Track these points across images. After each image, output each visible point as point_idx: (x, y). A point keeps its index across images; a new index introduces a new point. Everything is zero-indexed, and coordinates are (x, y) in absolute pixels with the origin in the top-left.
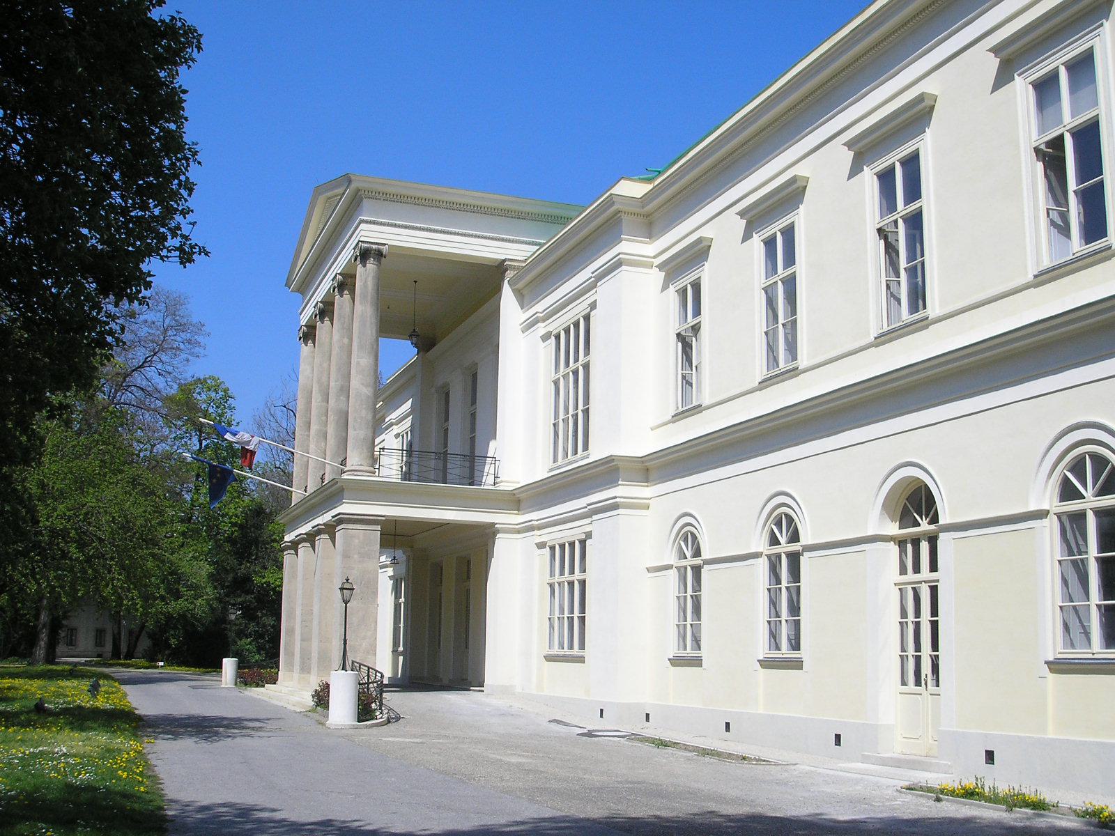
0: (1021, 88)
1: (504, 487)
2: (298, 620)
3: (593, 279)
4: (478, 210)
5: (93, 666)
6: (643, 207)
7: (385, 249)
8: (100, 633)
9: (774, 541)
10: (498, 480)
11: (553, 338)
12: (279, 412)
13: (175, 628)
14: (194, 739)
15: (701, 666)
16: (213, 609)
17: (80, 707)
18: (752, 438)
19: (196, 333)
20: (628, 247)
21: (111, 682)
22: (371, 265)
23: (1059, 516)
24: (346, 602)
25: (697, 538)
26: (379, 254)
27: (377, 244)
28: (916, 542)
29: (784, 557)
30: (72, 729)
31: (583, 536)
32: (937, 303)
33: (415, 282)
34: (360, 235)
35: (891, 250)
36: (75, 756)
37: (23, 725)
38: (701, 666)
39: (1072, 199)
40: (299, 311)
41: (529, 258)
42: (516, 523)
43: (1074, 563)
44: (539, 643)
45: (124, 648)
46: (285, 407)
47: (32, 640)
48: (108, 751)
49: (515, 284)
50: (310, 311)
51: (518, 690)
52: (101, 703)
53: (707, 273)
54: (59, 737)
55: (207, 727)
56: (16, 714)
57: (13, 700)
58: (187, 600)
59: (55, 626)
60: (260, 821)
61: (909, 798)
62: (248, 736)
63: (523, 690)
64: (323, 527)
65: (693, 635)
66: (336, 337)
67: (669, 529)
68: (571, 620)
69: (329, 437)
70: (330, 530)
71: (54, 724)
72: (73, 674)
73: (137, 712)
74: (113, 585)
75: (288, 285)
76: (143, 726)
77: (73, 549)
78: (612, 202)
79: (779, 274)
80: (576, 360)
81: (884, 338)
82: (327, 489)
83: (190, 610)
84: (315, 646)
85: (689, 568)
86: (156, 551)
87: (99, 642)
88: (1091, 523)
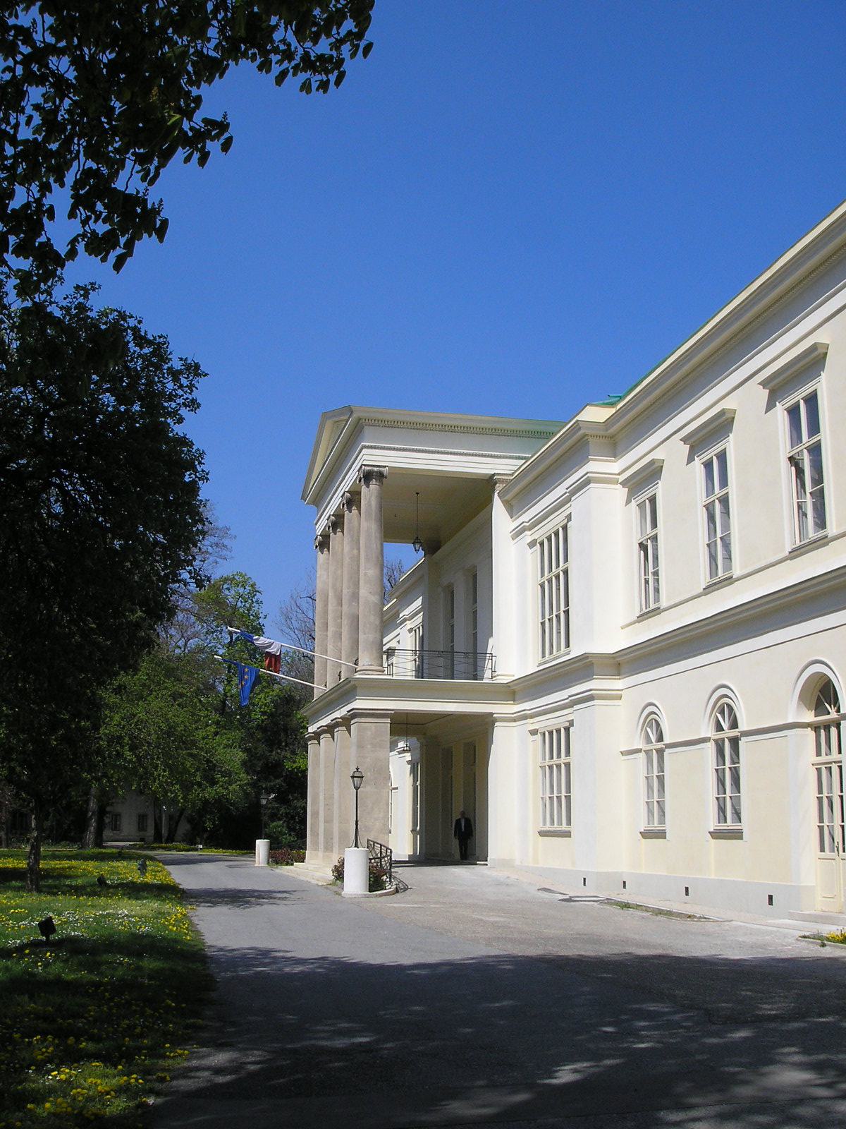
3: (567, 494)
4: (467, 430)
6: (607, 430)
7: (385, 470)
8: (142, 819)
9: (719, 728)
10: (495, 674)
11: (538, 545)
12: (304, 604)
13: (211, 813)
14: (229, 906)
15: (570, 837)
16: (246, 794)
17: (132, 882)
18: (708, 635)
20: (596, 466)
22: (374, 485)
24: (357, 788)
25: (733, 709)
26: (381, 476)
27: (378, 466)
28: (827, 727)
30: (129, 898)
31: (567, 724)
32: (834, 523)
33: (417, 494)
35: (800, 473)
36: (134, 916)
38: (570, 837)
41: (516, 471)
42: (513, 712)
44: (535, 820)
45: (164, 831)
46: (310, 598)
47: (82, 826)
48: (160, 913)
49: (504, 496)
51: (517, 863)
52: (149, 879)
53: (661, 489)
55: (240, 897)
57: (77, 877)
58: (222, 786)
59: (102, 812)
60: (275, 958)
61: (803, 944)
62: (274, 904)
63: (521, 862)
64: (340, 720)
65: (733, 806)
66: (347, 549)
67: (637, 719)
68: (559, 798)
70: (346, 722)
72: (120, 856)
73: (180, 887)
75: (304, 498)
76: (187, 897)
77: (128, 754)
78: (577, 428)
79: (804, 443)
80: (558, 566)
81: (796, 553)
82: (343, 686)
83: (226, 795)
85: (726, 740)
86: (194, 751)
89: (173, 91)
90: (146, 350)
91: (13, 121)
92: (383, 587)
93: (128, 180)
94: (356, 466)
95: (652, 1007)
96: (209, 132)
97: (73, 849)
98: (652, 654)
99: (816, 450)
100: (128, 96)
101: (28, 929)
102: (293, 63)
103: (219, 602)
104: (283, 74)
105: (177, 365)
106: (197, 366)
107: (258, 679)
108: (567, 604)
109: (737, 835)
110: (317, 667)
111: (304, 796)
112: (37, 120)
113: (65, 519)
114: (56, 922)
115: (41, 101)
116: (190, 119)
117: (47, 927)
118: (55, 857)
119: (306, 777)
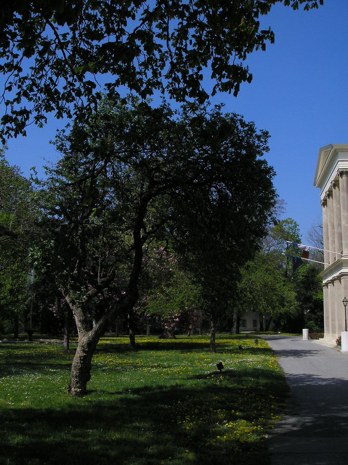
2: (330, 313)
5: (254, 334)
8: (255, 322)
12: (318, 229)
19: (282, 204)
21: (262, 340)
22: (344, 177)
24: (345, 306)
34: (339, 166)
36: (254, 362)
37: (236, 353)
40: (320, 195)
45: (264, 327)
47: (231, 325)
52: (259, 346)
54: (249, 356)
55: (298, 353)
56: (233, 350)
57: (230, 346)
58: (287, 307)
59: (239, 319)
69: (336, 243)
70: (339, 278)
71: (246, 352)
72: (247, 337)
73: (272, 349)
74: (262, 305)
76: (275, 354)
77: (248, 294)
82: (336, 263)
86: (276, 293)
87: (255, 325)
90: (245, 129)
91: (184, 44)
93: (234, 60)
94: (336, 170)
97: (227, 335)
101: (210, 367)
103: (282, 231)
105: (258, 133)
112: (194, 41)
114: (223, 364)
117: (220, 366)
118: (220, 338)
119: (322, 302)
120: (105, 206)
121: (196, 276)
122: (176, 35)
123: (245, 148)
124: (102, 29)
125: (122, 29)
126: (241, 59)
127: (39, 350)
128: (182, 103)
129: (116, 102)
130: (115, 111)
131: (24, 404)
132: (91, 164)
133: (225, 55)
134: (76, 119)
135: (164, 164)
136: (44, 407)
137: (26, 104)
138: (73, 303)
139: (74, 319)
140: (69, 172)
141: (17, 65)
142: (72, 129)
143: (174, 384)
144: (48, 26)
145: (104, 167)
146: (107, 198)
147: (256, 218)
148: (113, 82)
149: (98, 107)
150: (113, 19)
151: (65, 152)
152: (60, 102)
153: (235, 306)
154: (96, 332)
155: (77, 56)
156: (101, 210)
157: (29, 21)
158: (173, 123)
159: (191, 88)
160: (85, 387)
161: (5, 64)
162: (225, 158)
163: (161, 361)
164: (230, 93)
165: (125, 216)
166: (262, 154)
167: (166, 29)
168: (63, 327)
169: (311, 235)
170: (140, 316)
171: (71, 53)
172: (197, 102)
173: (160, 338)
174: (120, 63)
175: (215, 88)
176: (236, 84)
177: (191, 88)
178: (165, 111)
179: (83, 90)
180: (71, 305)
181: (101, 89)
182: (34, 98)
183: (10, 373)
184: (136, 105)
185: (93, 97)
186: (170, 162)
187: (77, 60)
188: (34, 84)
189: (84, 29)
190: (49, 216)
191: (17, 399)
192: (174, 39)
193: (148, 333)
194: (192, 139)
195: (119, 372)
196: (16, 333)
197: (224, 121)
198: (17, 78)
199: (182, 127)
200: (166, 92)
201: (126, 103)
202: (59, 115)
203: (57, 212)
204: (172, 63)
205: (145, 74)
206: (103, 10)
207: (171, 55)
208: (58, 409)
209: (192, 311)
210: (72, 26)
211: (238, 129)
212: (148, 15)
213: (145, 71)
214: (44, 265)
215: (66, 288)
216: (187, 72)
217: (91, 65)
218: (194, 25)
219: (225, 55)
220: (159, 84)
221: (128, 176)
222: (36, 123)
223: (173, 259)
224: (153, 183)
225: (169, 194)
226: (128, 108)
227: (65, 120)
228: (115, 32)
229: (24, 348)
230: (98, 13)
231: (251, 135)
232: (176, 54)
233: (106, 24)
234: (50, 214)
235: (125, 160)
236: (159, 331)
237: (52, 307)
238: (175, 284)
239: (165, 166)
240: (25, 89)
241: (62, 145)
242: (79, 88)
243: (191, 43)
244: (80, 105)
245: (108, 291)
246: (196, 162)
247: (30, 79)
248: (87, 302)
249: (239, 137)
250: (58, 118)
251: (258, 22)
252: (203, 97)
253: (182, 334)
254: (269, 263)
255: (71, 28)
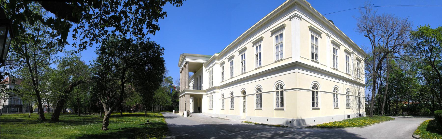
0: (274, 37)
1: (203, 90)
4: (199, 57)
8: (159, 108)
9: (231, 96)
12: (179, 80)
15: (262, 110)
16: (172, 105)
18: (230, 84)
20: (216, 62)
22: (187, 64)
23: (276, 92)
26: (188, 63)
28: (244, 97)
29: (280, 92)
35: (242, 64)
38: (262, 110)
39: (259, 60)
43: (278, 97)
44: (208, 107)
45: (161, 109)
47: (151, 109)
50: (181, 69)
52: (160, 115)
56: (152, 116)
59: (154, 107)
70: (184, 95)
72: (156, 113)
75: (178, 66)
77: (157, 99)
81: (241, 74)
84: (183, 108)
87: (159, 109)
88: (280, 92)
89: (158, 7)
90: (157, 47)
91: (137, 16)
92: (189, 78)
93: (154, 22)
94: (185, 62)
95: (222, 130)
96: (164, 14)
97: (150, 112)
98: (223, 87)
99: (245, 61)
100: (152, 9)
101: (145, 122)
102: (175, 2)
103: (168, 80)
104: (174, 4)
105: (161, 48)
106: (164, 49)
107: (173, 90)
108: (212, 80)
109: (233, 110)
110: (180, 88)
111: (179, 105)
112: (141, 15)
113: (148, 70)
114: (149, 121)
115: (141, 11)
116: (161, 12)
117: (148, 121)
118: (148, 113)
119: (179, 102)
120: (112, 72)
121: (141, 94)
122: (135, 12)
123: (157, 53)
124: (110, 10)
125: (116, 10)
126: (157, 22)
127: (93, 117)
128: (137, 37)
129: (115, 37)
130: (115, 40)
131: (90, 133)
132: (108, 58)
133: (151, 20)
134: (102, 43)
135: (131, 58)
136: (95, 133)
137: (87, 39)
138: (103, 102)
139: (103, 108)
140: (101, 61)
141: (83, 26)
142: (101, 47)
143: (134, 127)
144: (91, 10)
145: (112, 59)
146: (113, 69)
147: (160, 76)
148: (114, 30)
149: (109, 39)
150: (113, 6)
151: (99, 55)
152: (97, 38)
153: (153, 103)
154: (110, 111)
155: (102, 21)
156: (111, 73)
157: (84, 7)
158: (134, 44)
159: (140, 32)
160: (107, 128)
161: (80, 26)
162: (150, 56)
163: (130, 120)
164: (152, 34)
165: (118, 75)
166: (162, 55)
167: (131, 10)
168: (100, 110)
169: (177, 82)
170: (124, 106)
171: (100, 20)
172: (142, 37)
173: (130, 113)
174: (116, 23)
175: (147, 32)
176: (154, 31)
177: (140, 32)
178: (131, 40)
179: (104, 33)
180: (102, 103)
181: (110, 33)
182: (89, 37)
183: (85, 124)
184: (122, 38)
185: (107, 35)
186: (133, 57)
187: (102, 22)
188: (89, 32)
189: (103, 10)
190: (95, 76)
191: (88, 132)
192: (134, 14)
193: (126, 111)
194: (140, 49)
195: (117, 123)
196: (86, 112)
197: (150, 44)
198: (84, 31)
199: (137, 45)
200: (131, 33)
201: (118, 37)
202: (97, 42)
203: (97, 74)
204: (133, 23)
205: (125, 27)
206: (110, 2)
207: (133, 20)
208: (99, 134)
209: (140, 104)
210: (99, 9)
211: (154, 47)
212: (125, 4)
213: (124, 26)
214: (94, 91)
215: (101, 98)
216: (138, 26)
217: (106, 24)
218: (141, 8)
219: (151, 20)
220: (129, 30)
221: (119, 62)
222: (90, 46)
223: (133, 89)
224: (127, 64)
225: (132, 68)
226: (119, 39)
227: (99, 44)
228: (114, 11)
229: (88, 117)
230: (108, 3)
231: (159, 49)
232: (135, 19)
233: (111, 8)
234: (95, 75)
235: (118, 57)
236: (129, 111)
237: (96, 104)
238: (134, 96)
239: (131, 59)
240: (86, 34)
241: (98, 52)
242: (103, 32)
243: (140, 15)
244: (103, 38)
245: (114, 98)
246: (141, 57)
247: (88, 30)
248: (107, 102)
249: (155, 49)
250: (96, 43)
251: (162, 8)
252: (143, 35)
253: (136, 111)
254: (163, 90)
255: (99, 10)
